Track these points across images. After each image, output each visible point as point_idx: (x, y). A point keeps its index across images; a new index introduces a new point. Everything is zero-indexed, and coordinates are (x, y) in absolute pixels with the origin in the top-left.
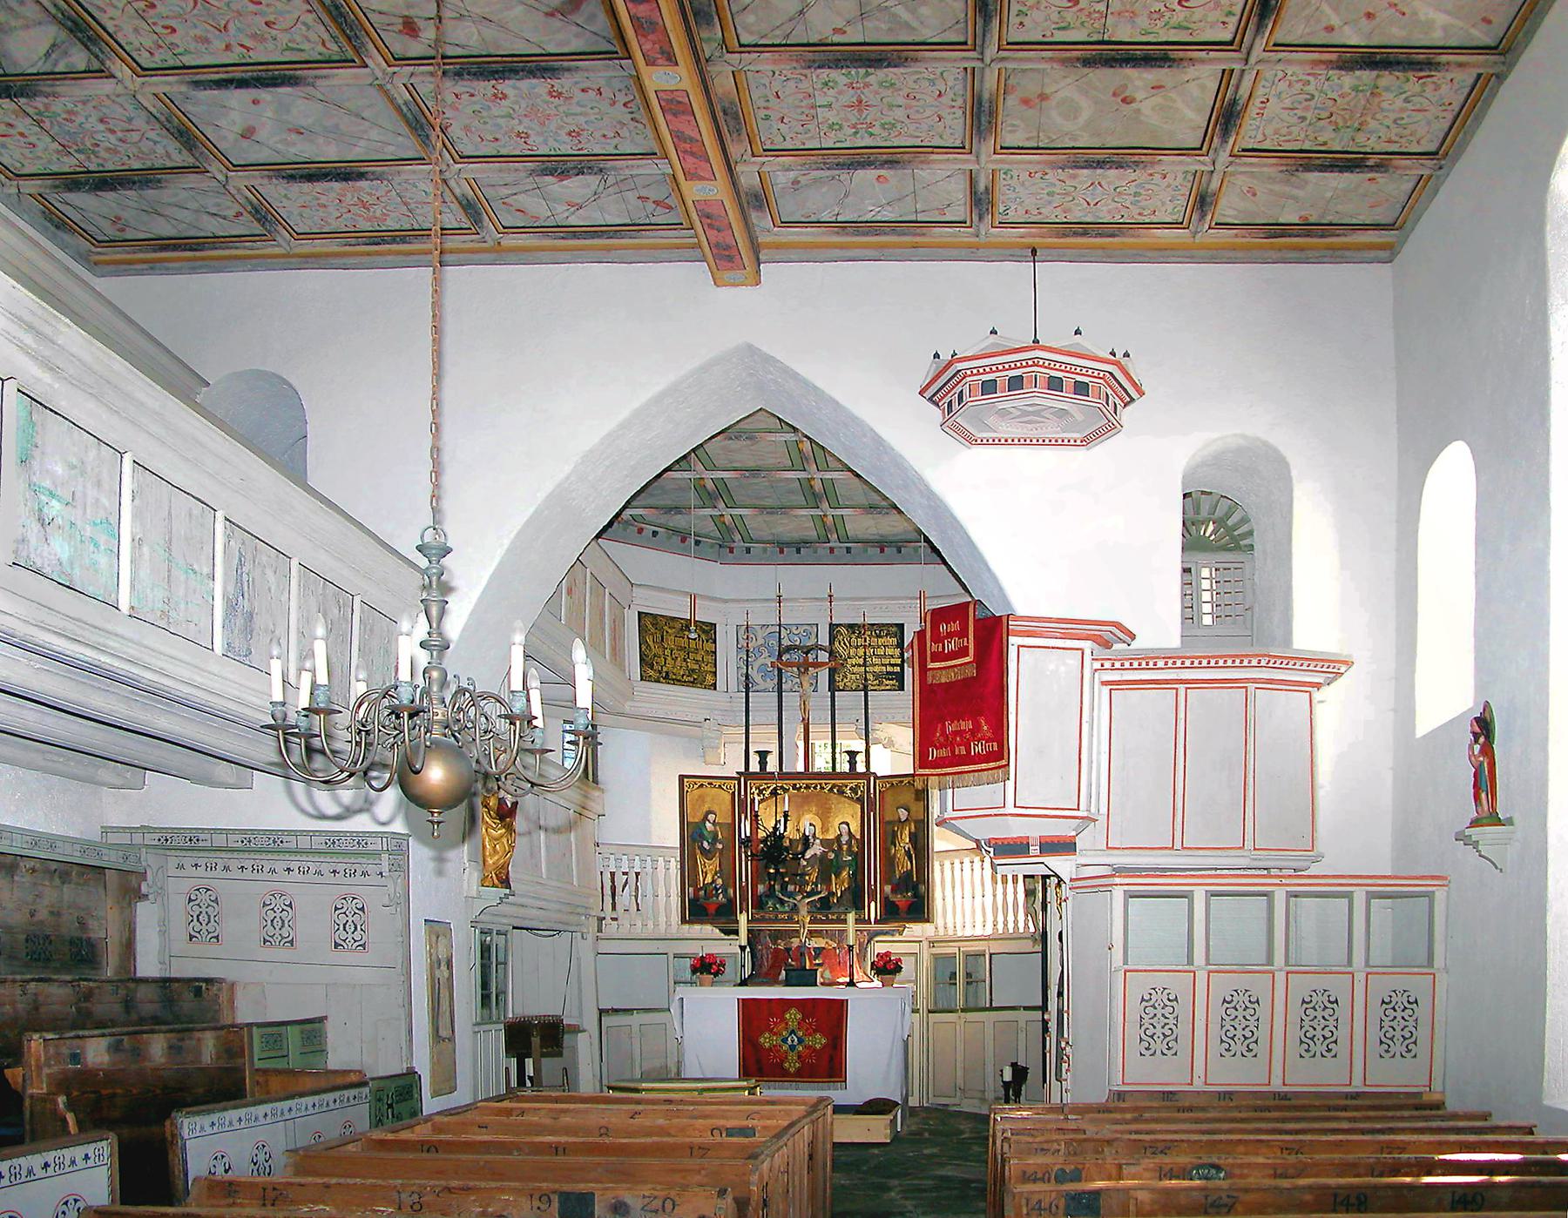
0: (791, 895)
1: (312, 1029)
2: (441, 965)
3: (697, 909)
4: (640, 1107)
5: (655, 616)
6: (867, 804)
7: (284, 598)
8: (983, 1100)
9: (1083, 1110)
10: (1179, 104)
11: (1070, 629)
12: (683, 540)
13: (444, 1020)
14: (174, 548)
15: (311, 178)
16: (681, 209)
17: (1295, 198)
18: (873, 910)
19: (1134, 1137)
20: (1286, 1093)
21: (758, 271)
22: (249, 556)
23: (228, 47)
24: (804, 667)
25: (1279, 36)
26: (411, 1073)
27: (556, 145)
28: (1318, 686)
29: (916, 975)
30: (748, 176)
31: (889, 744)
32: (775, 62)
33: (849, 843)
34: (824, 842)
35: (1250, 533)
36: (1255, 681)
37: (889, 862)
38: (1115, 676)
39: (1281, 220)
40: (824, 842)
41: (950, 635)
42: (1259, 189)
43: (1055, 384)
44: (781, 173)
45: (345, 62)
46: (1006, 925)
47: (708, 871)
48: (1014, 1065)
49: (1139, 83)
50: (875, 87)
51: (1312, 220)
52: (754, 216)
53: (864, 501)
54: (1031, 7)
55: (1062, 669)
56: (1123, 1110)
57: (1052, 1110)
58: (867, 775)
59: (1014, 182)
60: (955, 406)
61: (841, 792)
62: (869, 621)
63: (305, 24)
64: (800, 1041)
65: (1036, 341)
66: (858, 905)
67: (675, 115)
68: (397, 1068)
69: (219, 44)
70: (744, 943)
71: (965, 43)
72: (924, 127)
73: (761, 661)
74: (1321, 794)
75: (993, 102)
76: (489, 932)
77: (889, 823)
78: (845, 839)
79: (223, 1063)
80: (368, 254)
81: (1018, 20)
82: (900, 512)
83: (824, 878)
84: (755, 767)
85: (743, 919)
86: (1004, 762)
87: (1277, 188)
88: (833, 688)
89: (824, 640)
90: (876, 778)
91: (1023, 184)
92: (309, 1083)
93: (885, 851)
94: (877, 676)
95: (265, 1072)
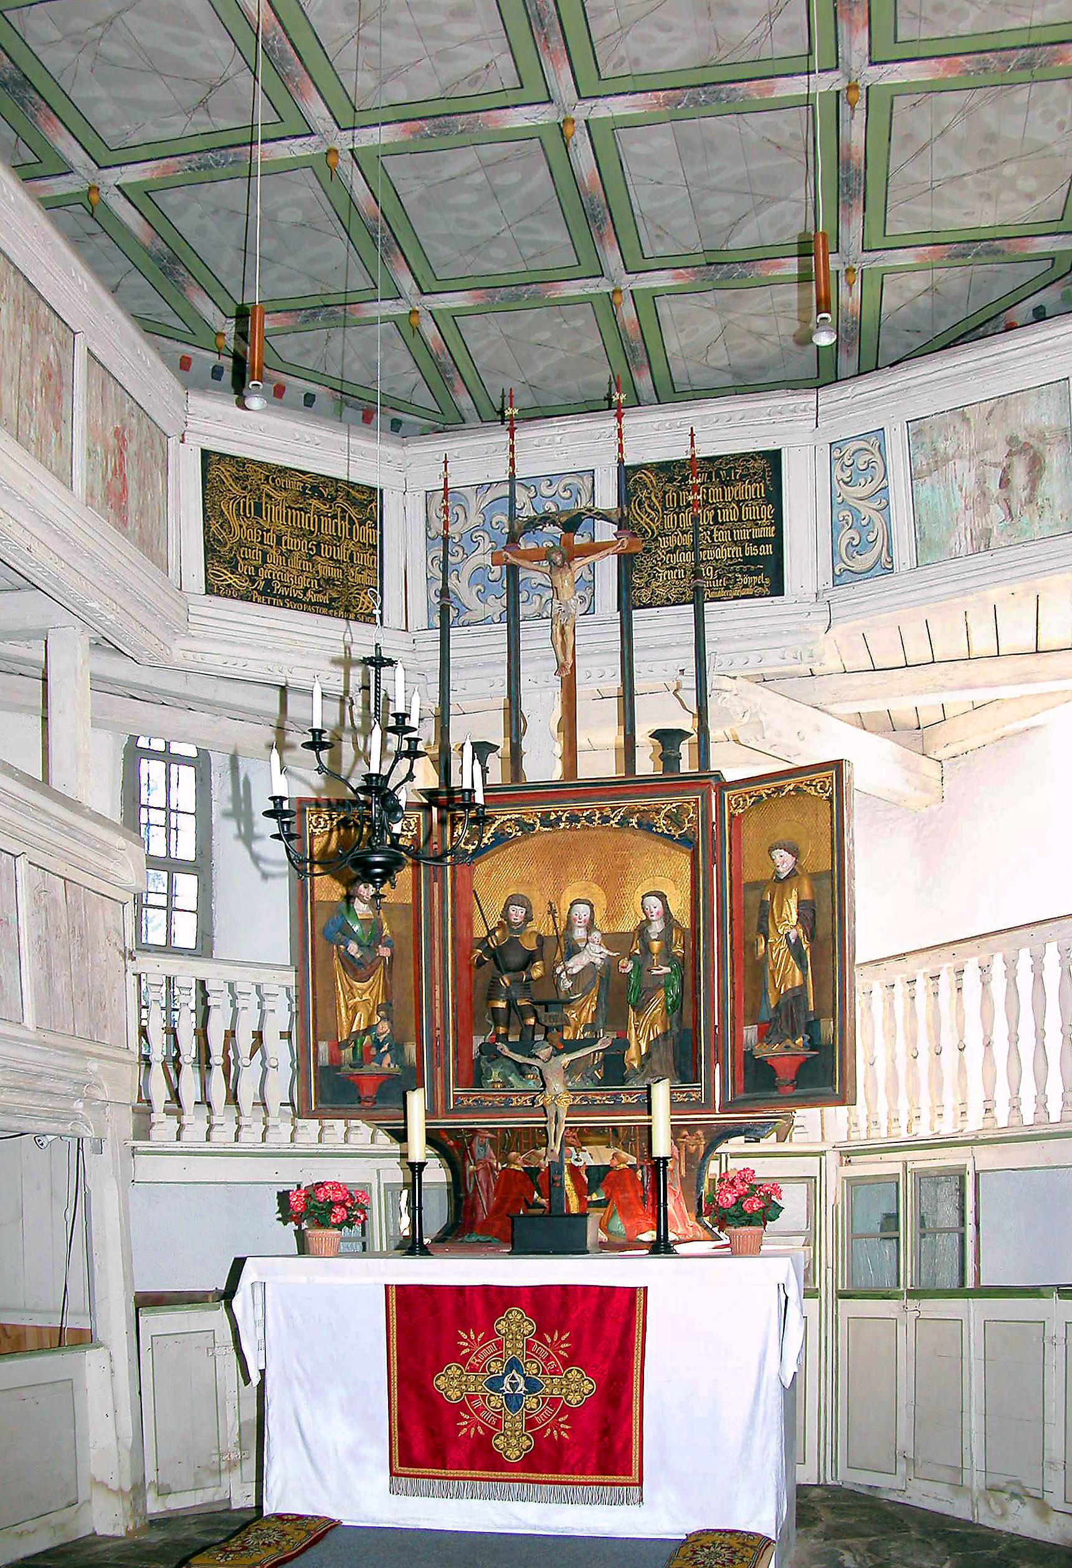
6: (701, 846)
8: (958, 1487)
33: (666, 938)
34: (610, 940)
46: (1015, 1108)
47: (358, 1005)
58: (707, 780)
64: (532, 1386)
77: (756, 885)
88: (627, 604)
89: (607, 498)
93: (744, 948)
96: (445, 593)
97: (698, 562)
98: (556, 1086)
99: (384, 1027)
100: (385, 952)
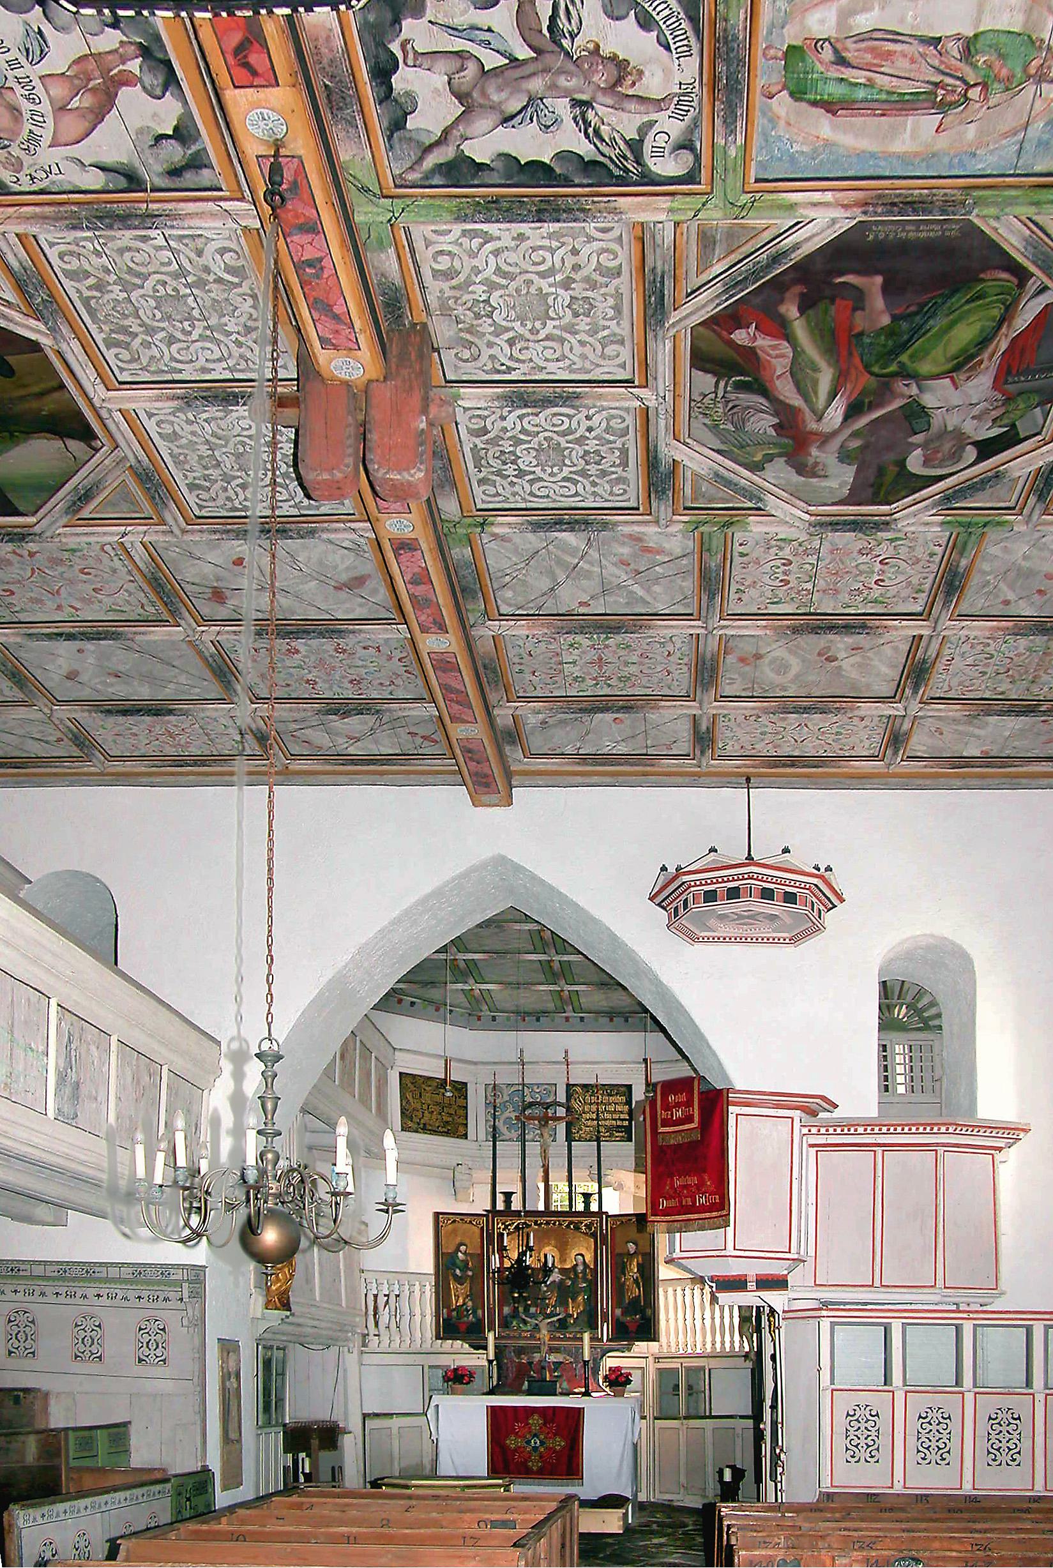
0: (533, 1316)
1: (118, 1432)
2: (230, 1377)
3: (450, 1327)
4: (414, 1502)
5: (414, 1076)
7: (105, 1069)
9: (799, 1508)
10: (876, 663)
11: (781, 1101)
12: (437, 1010)
13: (233, 1426)
14: (16, 1032)
15: (125, 713)
16: (444, 742)
17: (979, 737)
18: (605, 1331)
19: (843, 1533)
20: (976, 1496)
21: (511, 796)
22: (76, 1036)
23: (59, 607)
24: (544, 1121)
25: (964, 608)
26: (206, 1470)
27: (340, 691)
28: (1000, 1149)
29: (644, 1384)
30: (504, 715)
31: (619, 1187)
32: (529, 628)
33: (584, 1272)
35: (939, 1016)
36: (944, 1145)
37: (619, 1290)
38: (821, 1140)
39: (965, 754)
40: (563, 1271)
41: (678, 1105)
42: (945, 730)
43: (767, 894)
44: (531, 715)
45: (221, 700)
48: (733, 1468)
49: (840, 646)
50: (614, 648)
51: (992, 754)
52: (507, 749)
53: (595, 979)
54: (749, 586)
55: (775, 1134)
56: (832, 1510)
57: (770, 1509)
58: (600, 1213)
59: (732, 724)
60: (681, 911)
61: (577, 1228)
62: (601, 1082)
63: (126, 591)
65: (749, 857)
66: (593, 1326)
67: (444, 672)
68: (194, 1466)
69: (50, 604)
70: (491, 1357)
71: (691, 615)
72: (655, 680)
73: (507, 1114)
74: (1003, 1241)
75: (715, 659)
76: (271, 1347)
77: (621, 1255)
78: (580, 1268)
79: (42, 1463)
80: (172, 774)
81: (737, 596)
82: (625, 988)
83: (562, 1302)
84: (500, 1206)
85: (491, 1337)
86: (724, 1213)
87: (960, 728)
88: (570, 1139)
89: (562, 1098)
90: (608, 1216)
91: (739, 725)
92: (118, 1480)
94: (609, 1129)
95: (79, 1469)
96: (494, 1127)
97: (598, 1125)
98: (544, 1332)
99: (470, 1303)
100: (470, 1273)
